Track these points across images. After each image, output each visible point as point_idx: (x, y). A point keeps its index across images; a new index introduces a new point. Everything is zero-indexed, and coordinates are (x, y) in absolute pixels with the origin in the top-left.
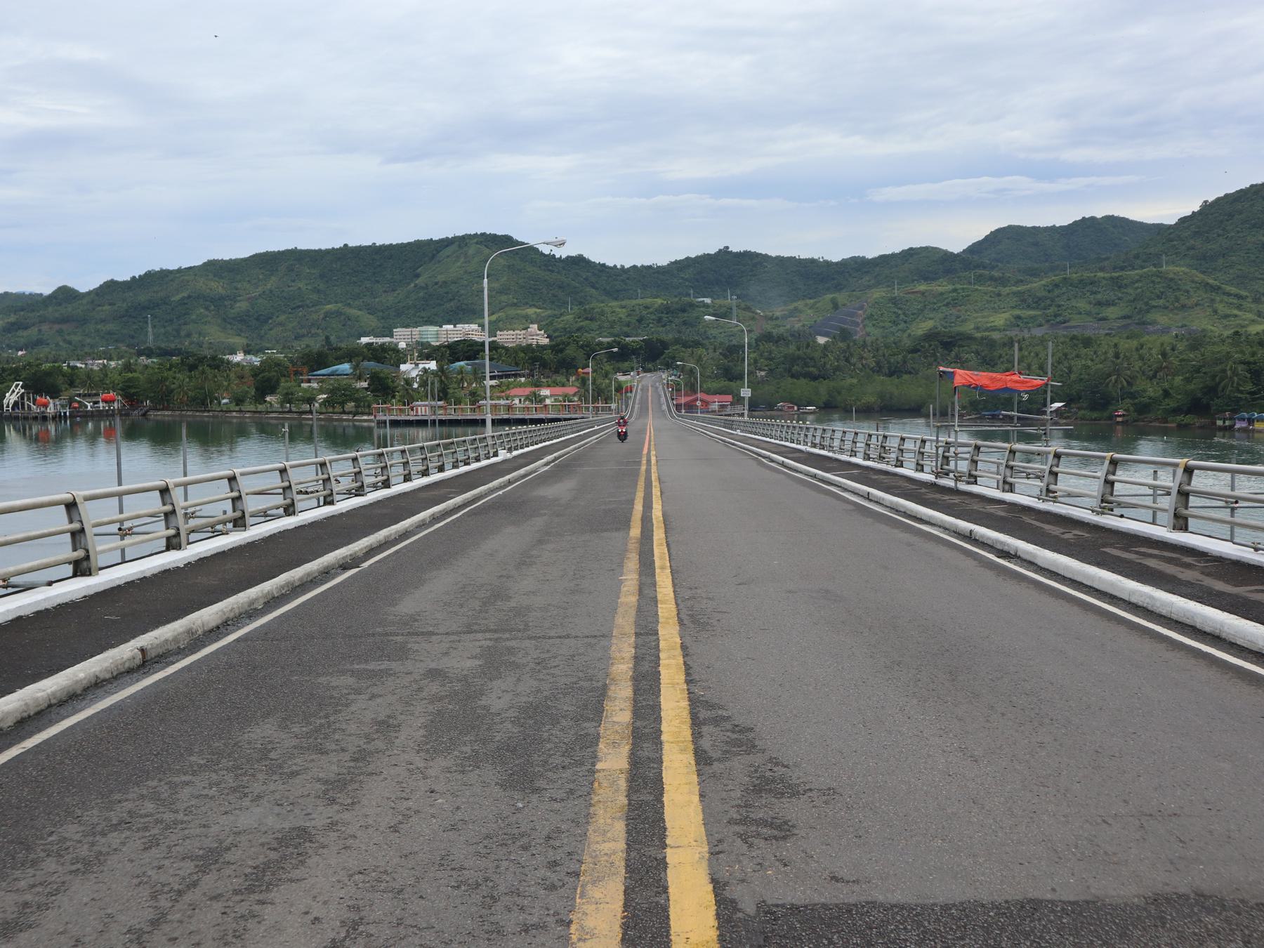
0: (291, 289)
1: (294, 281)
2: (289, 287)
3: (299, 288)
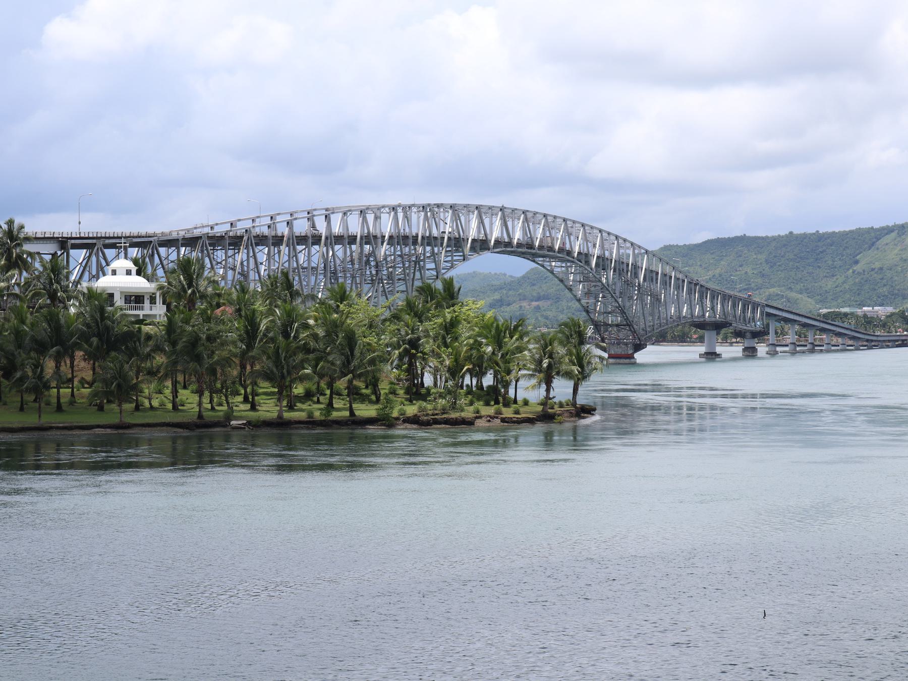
0: (738, 273)
1: (741, 266)
2: (736, 271)
3: (746, 273)
